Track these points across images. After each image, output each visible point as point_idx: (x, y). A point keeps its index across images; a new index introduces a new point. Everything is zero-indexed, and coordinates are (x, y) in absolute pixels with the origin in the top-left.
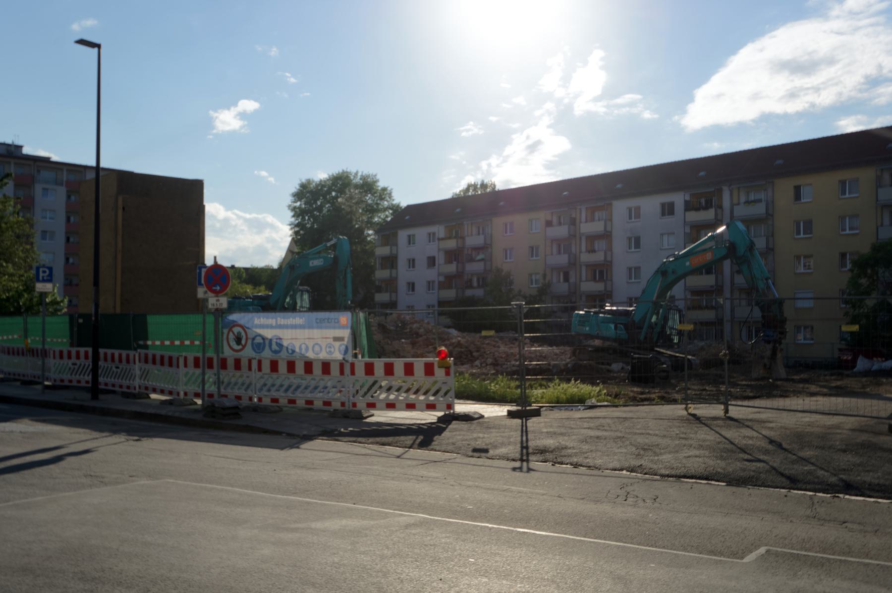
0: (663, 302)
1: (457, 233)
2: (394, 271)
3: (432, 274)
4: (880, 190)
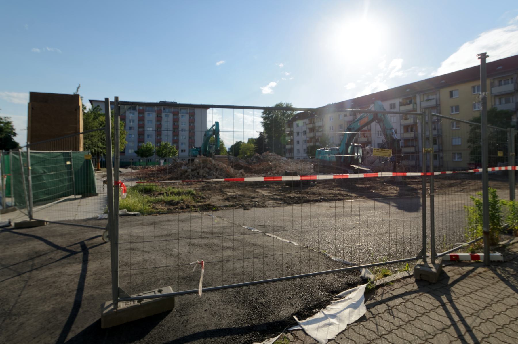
3: (304, 137)
4: (493, 89)
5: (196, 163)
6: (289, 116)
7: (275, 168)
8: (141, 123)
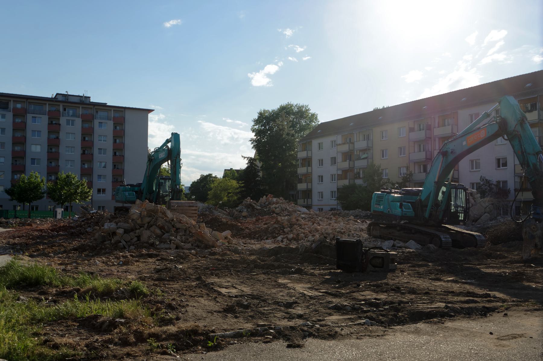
0: (447, 182)
1: (350, 139)
2: (309, 168)
3: (333, 170)
5: (135, 217)
6: (303, 129)
7: (291, 227)
8: (18, 134)
